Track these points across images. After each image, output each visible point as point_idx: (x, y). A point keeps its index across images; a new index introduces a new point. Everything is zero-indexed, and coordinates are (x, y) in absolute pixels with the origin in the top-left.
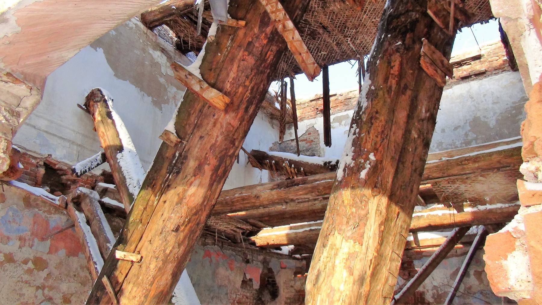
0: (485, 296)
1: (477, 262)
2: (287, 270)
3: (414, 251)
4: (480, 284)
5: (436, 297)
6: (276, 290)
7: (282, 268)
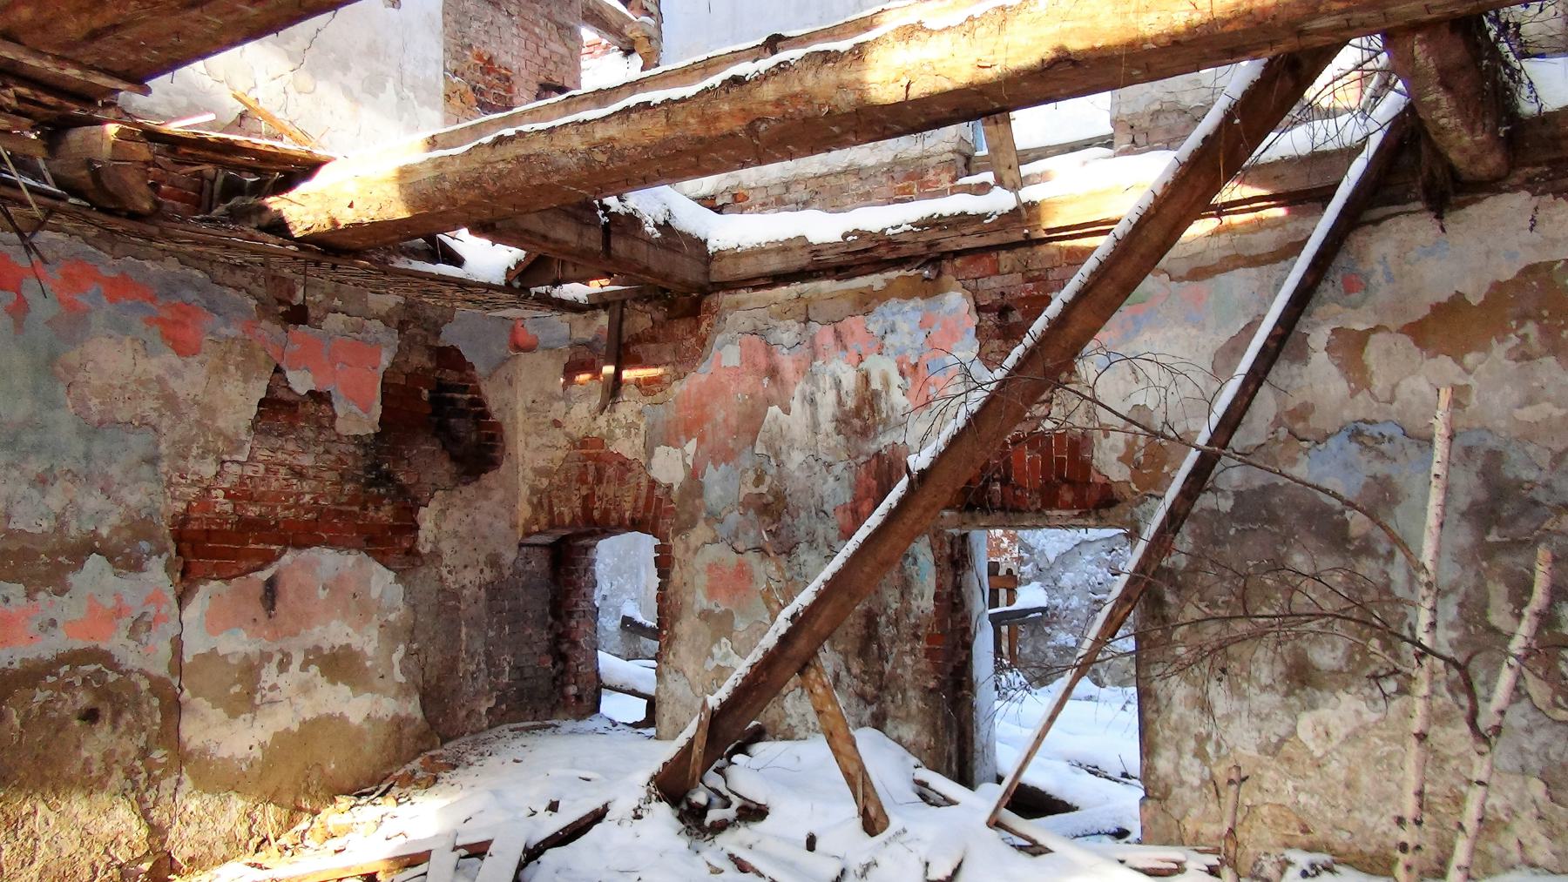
0: (1371, 448)
1: (1349, 288)
2: (538, 356)
3: (1060, 248)
4: (1353, 394)
5: (1140, 456)
6: (492, 437)
7: (518, 347)
